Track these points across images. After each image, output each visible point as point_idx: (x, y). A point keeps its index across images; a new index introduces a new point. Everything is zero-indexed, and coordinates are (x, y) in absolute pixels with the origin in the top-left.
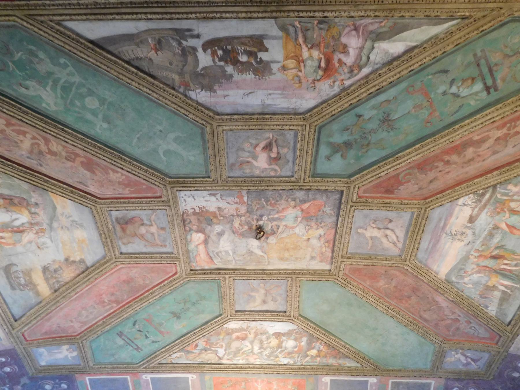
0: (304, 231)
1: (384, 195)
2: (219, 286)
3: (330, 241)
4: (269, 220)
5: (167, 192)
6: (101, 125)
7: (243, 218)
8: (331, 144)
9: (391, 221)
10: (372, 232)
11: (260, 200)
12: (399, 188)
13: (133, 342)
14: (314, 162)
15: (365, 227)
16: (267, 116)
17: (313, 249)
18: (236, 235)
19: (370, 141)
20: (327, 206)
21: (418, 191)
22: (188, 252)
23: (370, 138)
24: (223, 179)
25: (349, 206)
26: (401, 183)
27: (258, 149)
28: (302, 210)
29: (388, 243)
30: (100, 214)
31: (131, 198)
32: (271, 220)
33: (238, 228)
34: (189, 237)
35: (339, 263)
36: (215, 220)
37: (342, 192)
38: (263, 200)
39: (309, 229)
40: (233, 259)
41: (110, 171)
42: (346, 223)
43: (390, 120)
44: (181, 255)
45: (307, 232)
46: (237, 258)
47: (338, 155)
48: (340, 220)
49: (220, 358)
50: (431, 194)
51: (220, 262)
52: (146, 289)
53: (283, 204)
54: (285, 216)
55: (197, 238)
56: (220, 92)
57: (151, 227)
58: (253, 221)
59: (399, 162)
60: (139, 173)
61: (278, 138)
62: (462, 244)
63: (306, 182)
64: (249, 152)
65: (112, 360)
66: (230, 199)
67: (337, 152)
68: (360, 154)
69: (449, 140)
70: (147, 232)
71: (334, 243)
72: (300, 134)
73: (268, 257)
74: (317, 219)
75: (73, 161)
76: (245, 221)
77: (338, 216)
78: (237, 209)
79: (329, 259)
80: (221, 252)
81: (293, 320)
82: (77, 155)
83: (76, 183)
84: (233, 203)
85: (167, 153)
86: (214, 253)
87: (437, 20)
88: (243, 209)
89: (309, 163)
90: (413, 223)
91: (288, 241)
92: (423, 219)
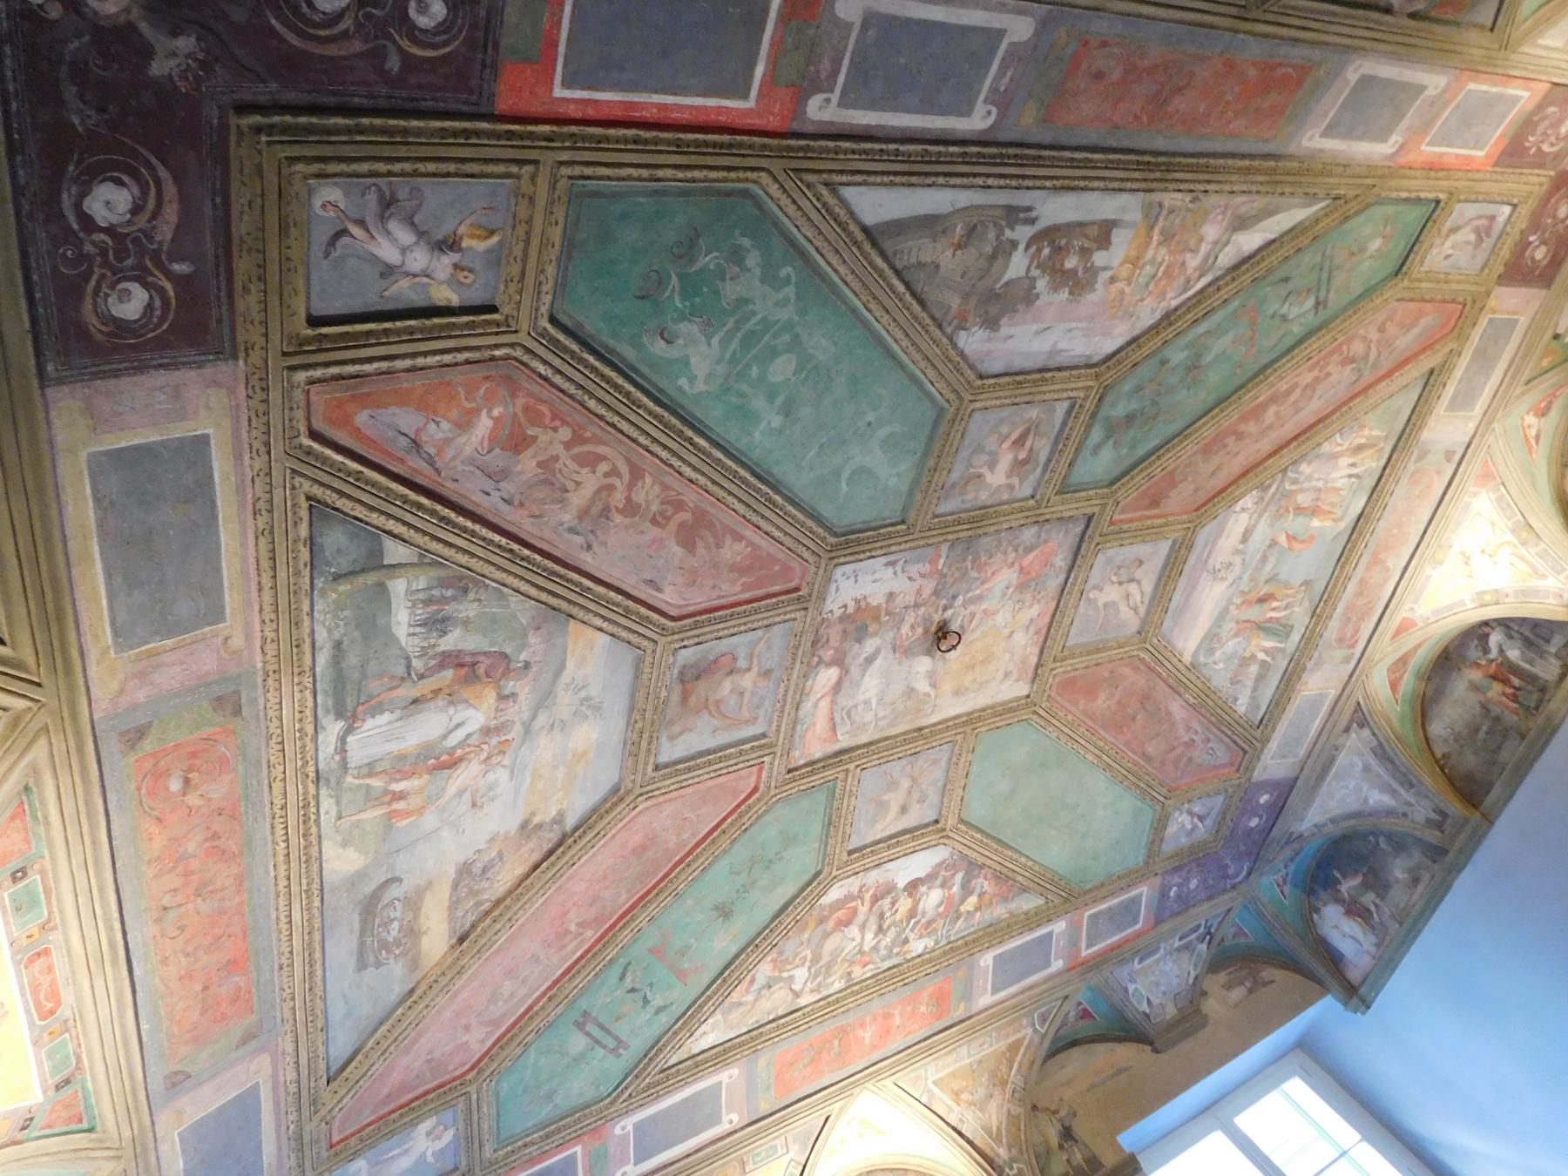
1: (1147, 513)
11: (965, 560)
13: (608, 1032)
16: (1049, 375)
27: (1006, 445)
49: (797, 995)
56: (1005, 330)
62: (1226, 584)
65: (544, 1112)
66: (914, 569)
75: (663, 527)
82: (679, 505)
85: (860, 473)
87: (1312, 198)
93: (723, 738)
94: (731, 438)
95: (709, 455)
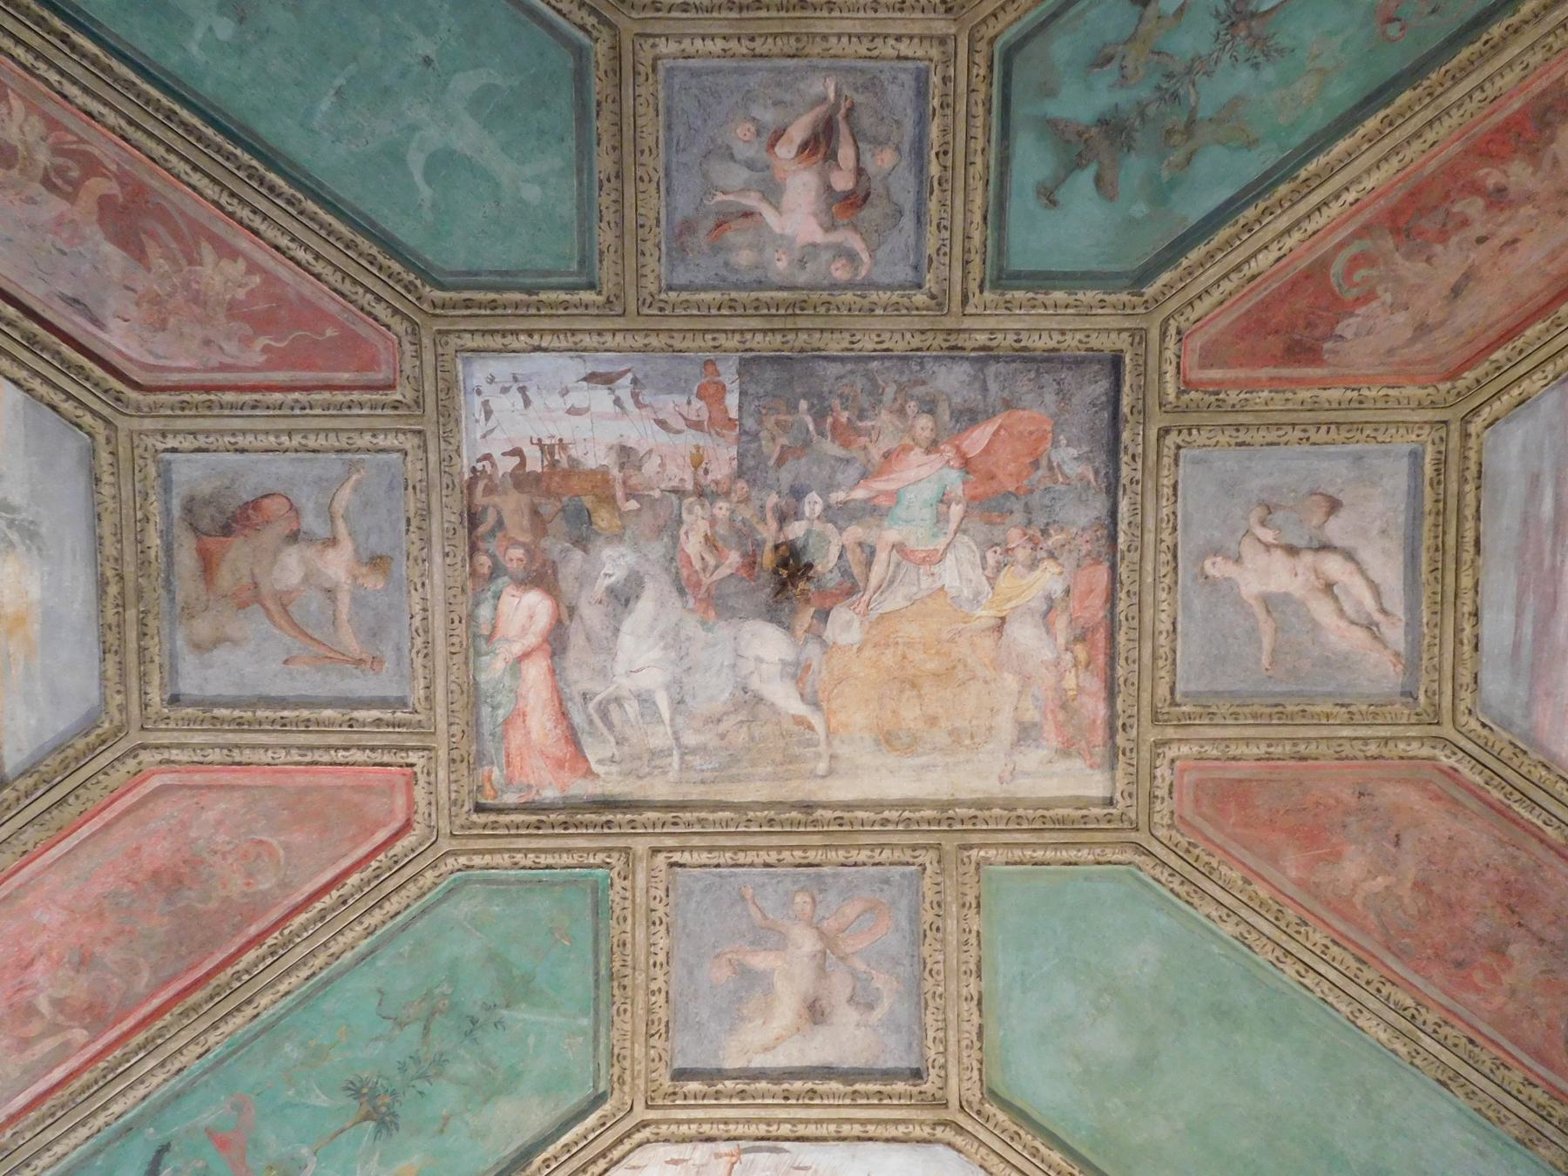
0: (977, 576)
1: (1285, 372)
2: (599, 909)
3: (1094, 630)
4: (831, 514)
5: (418, 355)
6: (210, 29)
7: (722, 509)
8: (1053, 129)
9: (1334, 506)
10: (1264, 574)
11: (793, 408)
12: (1339, 330)
14: (998, 214)
15: (1233, 546)
17: (1026, 680)
18: (691, 602)
19: (1193, 111)
20: (1063, 440)
21: (1412, 341)
22: (473, 696)
23: (1192, 99)
24: (645, 294)
25: (1153, 434)
26: (1340, 308)
28: (966, 464)
29: (1343, 624)
30: (125, 465)
31: (271, 388)
32: (837, 515)
33: (698, 565)
34: (484, 612)
35: (1145, 753)
36: (603, 519)
37: (1116, 362)
38: (803, 405)
39: (999, 568)
40: (670, 742)
41: (207, 251)
42: (1150, 523)
43: (1253, 15)
44: (441, 710)
45: (991, 581)
46: (690, 739)
47: (1084, 179)
48: (1124, 506)
50: (1467, 353)
51: (612, 760)
52: (253, 930)
53: (885, 428)
54: (895, 496)
55: (523, 613)
57: (331, 554)
58: (763, 520)
59: (1315, 199)
60: (318, 256)
61: (859, 98)
63: (970, 310)
64: (750, 165)
66: (670, 404)
67: (1078, 164)
68: (1165, 175)
69: (1481, 87)
70: (306, 579)
71: (1109, 636)
72: (935, 79)
73: (827, 722)
74: (1028, 509)
76: (732, 520)
77: (1112, 489)
78: (697, 461)
79: (1100, 735)
80: (618, 700)
81: (960, 1130)
82: (92, 166)
83: (59, 305)
84: (681, 425)
85: (443, 163)
86: (591, 706)
88: (723, 459)
89: (978, 218)
90: (1428, 505)
91: (910, 630)
92: (1463, 480)
93: (306, 682)
94: (149, 51)
95: (108, 70)
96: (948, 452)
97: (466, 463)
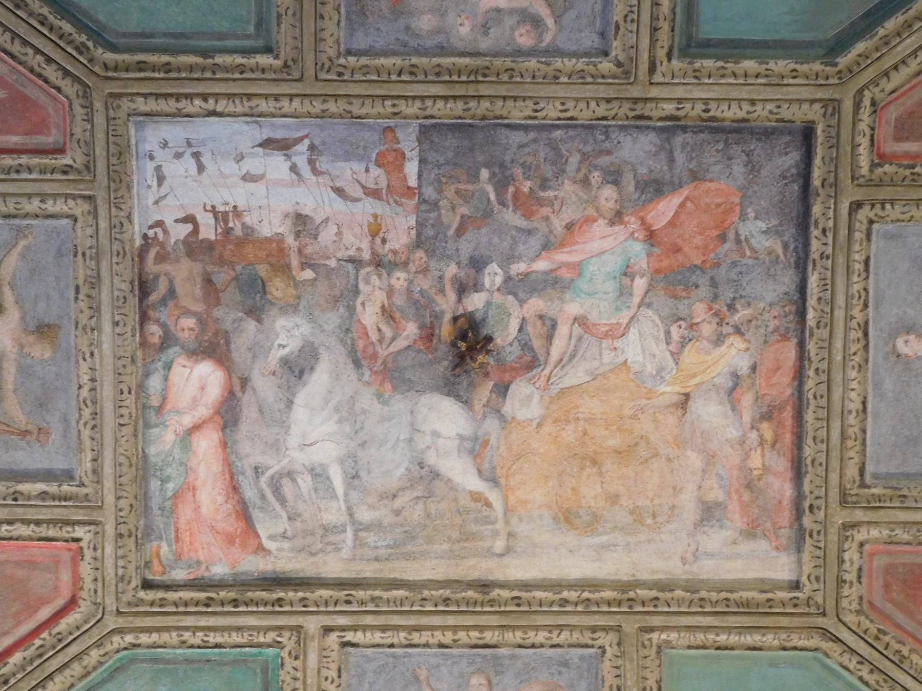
28: (651, 236)
54: (577, 268)
66: (348, 172)
96: (633, 223)
97: (137, 229)
